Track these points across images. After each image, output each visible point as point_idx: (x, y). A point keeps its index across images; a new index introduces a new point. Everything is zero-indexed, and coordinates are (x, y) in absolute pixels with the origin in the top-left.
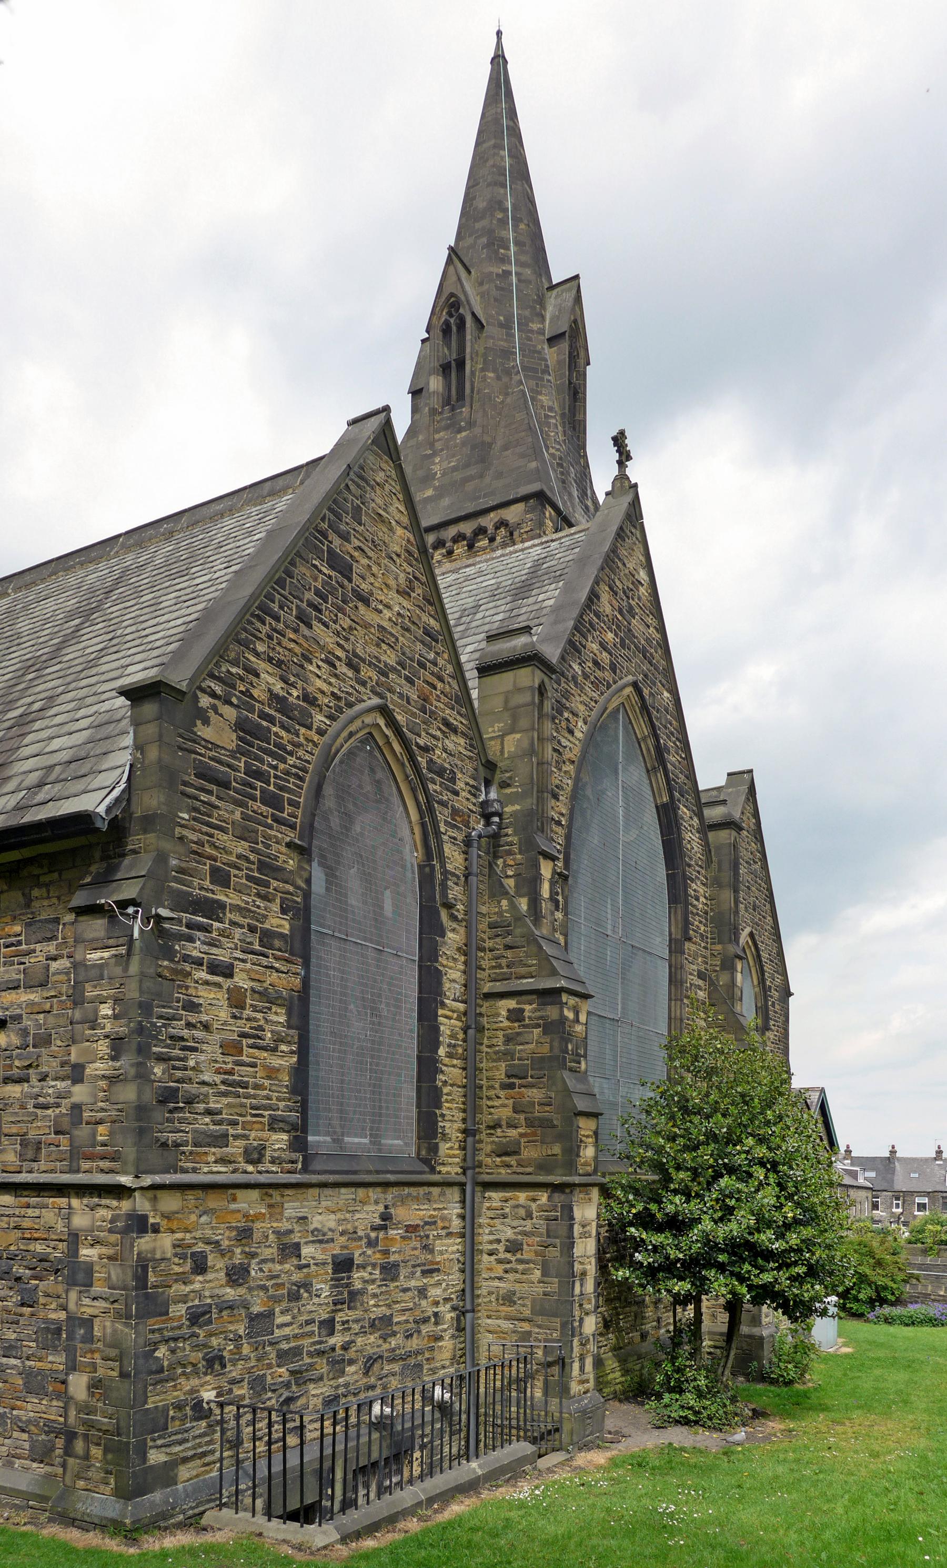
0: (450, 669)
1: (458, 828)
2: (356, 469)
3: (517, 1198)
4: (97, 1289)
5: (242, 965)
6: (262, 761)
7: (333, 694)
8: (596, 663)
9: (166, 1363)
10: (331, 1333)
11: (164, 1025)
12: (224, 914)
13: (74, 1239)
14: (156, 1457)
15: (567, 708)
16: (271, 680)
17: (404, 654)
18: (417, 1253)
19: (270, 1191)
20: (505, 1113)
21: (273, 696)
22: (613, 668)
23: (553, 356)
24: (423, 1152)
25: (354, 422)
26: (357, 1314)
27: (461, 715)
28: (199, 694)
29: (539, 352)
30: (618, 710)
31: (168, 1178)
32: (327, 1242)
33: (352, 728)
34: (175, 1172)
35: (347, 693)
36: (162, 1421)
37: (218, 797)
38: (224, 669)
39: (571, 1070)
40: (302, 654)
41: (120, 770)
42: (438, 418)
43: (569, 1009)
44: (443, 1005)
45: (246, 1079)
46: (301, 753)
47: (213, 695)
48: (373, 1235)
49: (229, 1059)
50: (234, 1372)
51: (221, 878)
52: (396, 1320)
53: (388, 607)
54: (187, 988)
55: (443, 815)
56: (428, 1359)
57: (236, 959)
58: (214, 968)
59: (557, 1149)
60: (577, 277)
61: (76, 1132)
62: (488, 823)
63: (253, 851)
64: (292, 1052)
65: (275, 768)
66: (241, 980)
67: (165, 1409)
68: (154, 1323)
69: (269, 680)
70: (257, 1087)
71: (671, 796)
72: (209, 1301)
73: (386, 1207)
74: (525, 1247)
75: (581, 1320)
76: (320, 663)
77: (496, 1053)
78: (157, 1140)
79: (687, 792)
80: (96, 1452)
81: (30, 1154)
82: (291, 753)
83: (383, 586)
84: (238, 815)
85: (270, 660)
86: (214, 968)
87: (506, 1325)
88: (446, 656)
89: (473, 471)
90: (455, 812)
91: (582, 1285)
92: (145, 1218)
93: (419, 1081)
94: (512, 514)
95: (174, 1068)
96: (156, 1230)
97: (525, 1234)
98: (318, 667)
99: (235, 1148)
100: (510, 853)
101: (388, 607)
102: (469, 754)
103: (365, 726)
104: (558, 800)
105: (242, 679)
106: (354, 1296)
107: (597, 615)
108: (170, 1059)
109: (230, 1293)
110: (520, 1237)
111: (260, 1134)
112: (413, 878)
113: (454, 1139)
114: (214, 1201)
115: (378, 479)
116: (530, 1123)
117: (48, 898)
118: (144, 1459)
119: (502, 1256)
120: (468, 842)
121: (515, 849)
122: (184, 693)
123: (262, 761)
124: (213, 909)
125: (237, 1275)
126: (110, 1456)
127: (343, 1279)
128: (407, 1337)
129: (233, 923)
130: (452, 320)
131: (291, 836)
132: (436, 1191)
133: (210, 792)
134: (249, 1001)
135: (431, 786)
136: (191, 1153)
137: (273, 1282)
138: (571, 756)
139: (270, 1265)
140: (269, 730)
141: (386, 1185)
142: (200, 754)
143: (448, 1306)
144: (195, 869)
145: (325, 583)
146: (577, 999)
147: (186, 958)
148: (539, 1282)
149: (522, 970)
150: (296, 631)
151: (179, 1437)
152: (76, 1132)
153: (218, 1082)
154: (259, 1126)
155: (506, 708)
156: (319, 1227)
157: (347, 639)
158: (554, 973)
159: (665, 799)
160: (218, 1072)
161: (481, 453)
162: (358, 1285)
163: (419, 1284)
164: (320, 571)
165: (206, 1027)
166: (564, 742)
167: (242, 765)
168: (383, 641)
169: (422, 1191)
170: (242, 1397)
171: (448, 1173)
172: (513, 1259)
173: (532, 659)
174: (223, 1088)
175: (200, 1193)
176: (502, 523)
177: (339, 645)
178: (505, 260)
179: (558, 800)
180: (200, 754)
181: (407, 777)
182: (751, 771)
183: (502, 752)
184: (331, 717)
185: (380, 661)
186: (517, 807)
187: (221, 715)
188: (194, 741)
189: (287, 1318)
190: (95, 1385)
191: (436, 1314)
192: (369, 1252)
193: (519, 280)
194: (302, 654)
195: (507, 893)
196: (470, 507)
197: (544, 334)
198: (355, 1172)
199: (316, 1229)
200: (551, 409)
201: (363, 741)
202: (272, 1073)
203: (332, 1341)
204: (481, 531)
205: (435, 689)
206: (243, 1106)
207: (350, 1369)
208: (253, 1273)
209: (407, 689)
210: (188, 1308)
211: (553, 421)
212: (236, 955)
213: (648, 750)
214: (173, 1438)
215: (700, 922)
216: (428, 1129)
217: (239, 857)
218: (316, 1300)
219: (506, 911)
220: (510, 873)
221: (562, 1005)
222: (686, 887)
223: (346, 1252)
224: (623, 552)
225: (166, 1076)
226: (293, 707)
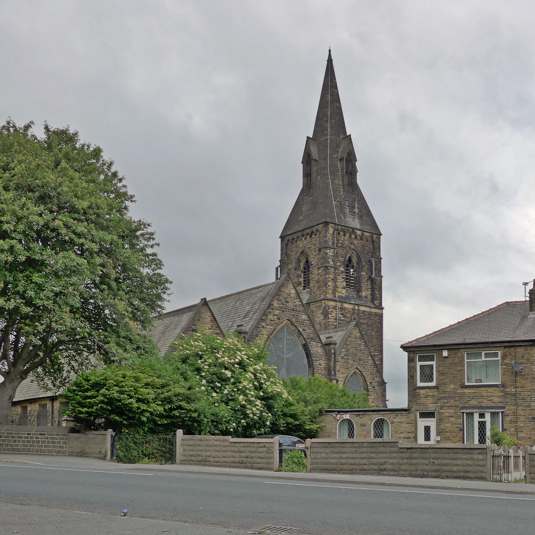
22: (279, 319)
193: (330, 141)
200: (339, 185)
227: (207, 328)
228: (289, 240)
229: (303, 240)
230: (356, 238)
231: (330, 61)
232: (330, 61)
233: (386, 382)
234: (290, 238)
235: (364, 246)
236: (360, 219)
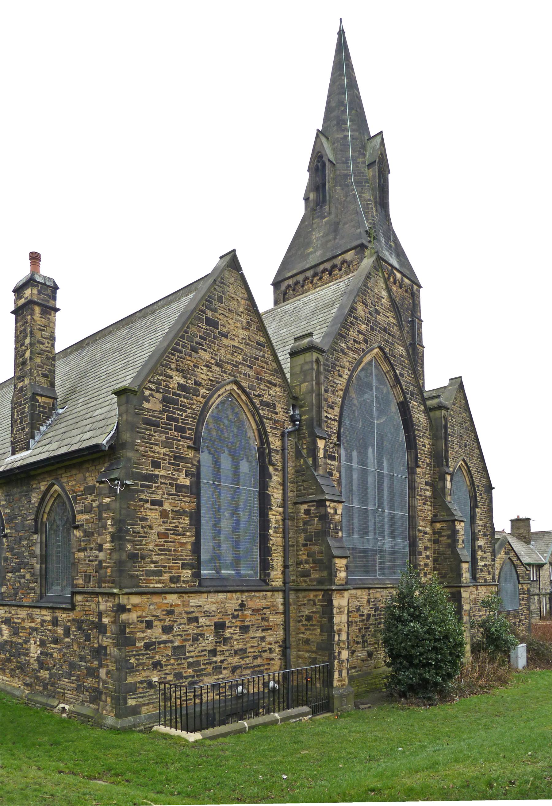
0: (271, 358)
1: (278, 429)
2: (219, 279)
3: (309, 596)
4: (108, 634)
5: (167, 501)
6: (175, 413)
7: (210, 380)
8: (355, 341)
9: (135, 665)
10: (215, 655)
11: (131, 528)
12: (158, 480)
13: (100, 615)
14: (131, 702)
15: (338, 366)
16: (178, 379)
17: (246, 356)
18: (259, 621)
19: (183, 595)
20: (304, 557)
21: (180, 386)
22: (366, 341)
23: (371, 173)
24: (263, 577)
25: (221, 258)
26: (226, 648)
27: (278, 378)
28: (145, 390)
29: (363, 173)
30: (372, 360)
31: (133, 590)
32: (212, 616)
33: (220, 392)
34: (137, 587)
35: (217, 378)
36: (134, 688)
37: (154, 432)
38: (156, 378)
39: (332, 536)
40: (194, 365)
41: (112, 426)
42: (314, 212)
43: (330, 508)
44: (271, 509)
45: (170, 548)
46: (194, 407)
47: (151, 389)
48: (236, 613)
49: (161, 540)
50: (167, 669)
51: (156, 465)
52: (248, 651)
53: (238, 337)
54: (141, 512)
55: (268, 424)
56: (266, 669)
57: (164, 498)
58: (154, 503)
59: (325, 574)
60: (382, 132)
61: (100, 572)
62: (294, 425)
63: (171, 451)
64: (192, 536)
65: (182, 415)
66: (167, 507)
67: (135, 683)
68: (129, 649)
69: (178, 379)
70: (174, 551)
71: (405, 398)
72: (154, 640)
73: (242, 601)
74: (313, 619)
75: (339, 653)
76: (203, 368)
77: (300, 530)
78: (129, 574)
79: (416, 394)
80: (109, 700)
81: (87, 580)
82: (189, 408)
83: (235, 328)
84: (163, 438)
85: (178, 370)
86: (154, 503)
87: (306, 654)
88: (269, 353)
89: (331, 237)
90: (276, 422)
91: (339, 636)
92: (124, 606)
93: (260, 544)
94: (349, 256)
95: (136, 545)
96: (129, 610)
97: (313, 612)
98: (202, 369)
99: (166, 577)
100: (304, 438)
101: (238, 337)
102: (283, 394)
103: (226, 391)
104: (334, 409)
105: (164, 381)
106: (226, 641)
107: (356, 318)
108: (135, 541)
109: (164, 637)
110: (311, 614)
111: (178, 571)
112: (255, 453)
113: (279, 570)
114: (156, 599)
115: (231, 282)
116: (314, 562)
117: (92, 477)
118: (126, 703)
119: (304, 623)
120: (283, 435)
121: (306, 436)
122: (137, 392)
123: (175, 413)
124: (153, 478)
125: (167, 630)
126: (113, 701)
127: (220, 632)
128: (254, 659)
129: (162, 483)
130: (319, 164)
131: (190, 443)
132: (269, 594)
133: (150, 430)
134: (170, 515)
135: (261, 412)
136: (144, 580)
137: (185, 633)
138: (341, 387)
139: (183, 626)
140: (178, 400)
141: (242, 592)
142: (145, 415)
143: (277, 645)
144: (144, 462)
145: (204, 333)
146: (335, 504)
147: (141, 500)
148: (320, 635)
149: (310, 491)
150: (190, 356)
151: (142, 695)
152: (100, 572)
153: (157, 550)
154: (177, 568)
155: (302, 371)
156: (208, 610)
157: (216, 355)
158: (323, 492)
159: (402, 399)
160: (156, 545)
161: (335, 228)
162: (228, 635)
163: (261, 635)
164: (202, 328)
165: (150, 527)
166: (338, 382)
167: (165, 417)
168: (235, 352)
169: (261, 594)
170: (171, 681)
171: (276, 585)
172: (309, 624)
173: (311, 348)
174: (159, 552)
175: (149, 596)
176: (344, 262)
177: (212, 357)
178: (346, 130)
179: (334, 409)
180: (145, 415)
181: (249, 410)
182: (461, 377)
183: (300, 392)
184: (209, 390)
185: (233, 361)
186: (307, 416)
187: (155, 397)
188: (142, 410)
189: (192, 649)
190: (108, 672)
191: (270, 649)
192: (234, 621)
193: (352, 139)
194: (194, 365)
195: (303, 456)
196: (329, 255)
197: (365, 163)
198: (226, 586)
199: (206, 611)
200: (369, 200)
201: (228, 397)
202: (182, 544)
203: (215, 659)
204: (334, 266)
205: (264, 368)
206: (169, 559)
207: (225, 672)
208: (175, 629)
209: (248, 371)
210: (145, 643)
211: (371, 206)
212: (164, 497)
213: (390, 377)
214: (139, 695)
215: (426, 457)
216: (265, 566)
217: (164, 455)
218: (207, 641)
219: (303, 465)
220: (305, 447)
221: (325, 506)
222: (415, 440)
223: (221, 620)
224: (370, 285)
225: (133, 548)
226: (190, 388)
227: (240, 325)
228: (289, 286)
229: (315, 281)
230: (395, 283)
231: (341, 33)
232: (341, 33)
233: (493, 486)
234: (291, 282)
235: (403, 299)
236: (397, 258)
